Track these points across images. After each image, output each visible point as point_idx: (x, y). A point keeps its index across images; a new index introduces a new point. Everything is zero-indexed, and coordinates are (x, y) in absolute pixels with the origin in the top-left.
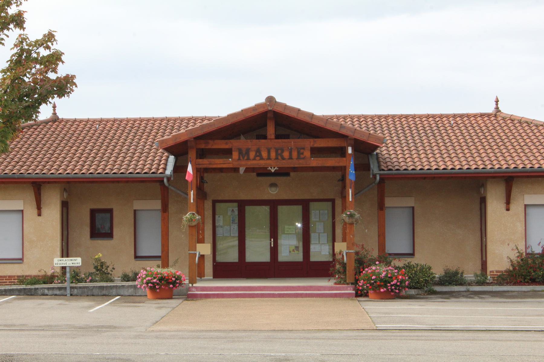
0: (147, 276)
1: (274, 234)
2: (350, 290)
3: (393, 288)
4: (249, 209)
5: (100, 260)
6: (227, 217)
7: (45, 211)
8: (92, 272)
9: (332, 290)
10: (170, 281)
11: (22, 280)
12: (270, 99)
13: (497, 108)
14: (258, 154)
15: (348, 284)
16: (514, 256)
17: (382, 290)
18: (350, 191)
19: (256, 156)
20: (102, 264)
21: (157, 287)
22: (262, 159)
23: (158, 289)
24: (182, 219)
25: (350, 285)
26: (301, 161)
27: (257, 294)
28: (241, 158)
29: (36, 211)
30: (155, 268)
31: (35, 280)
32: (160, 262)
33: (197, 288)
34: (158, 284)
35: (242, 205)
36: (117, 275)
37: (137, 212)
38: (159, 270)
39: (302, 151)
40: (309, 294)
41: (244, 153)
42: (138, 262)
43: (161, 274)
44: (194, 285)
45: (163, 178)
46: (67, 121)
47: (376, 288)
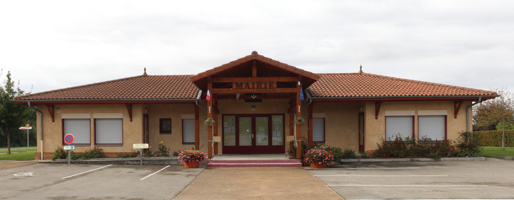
0: (184, 154)
1: (254, 131)
4: (241, 119)
6: (230, 122)
7: (134, 119)
11: (120, 155)
12: (255, 53)
13: (361, 71)
16: (380, 143)
20: (163, 147)
22: (249, 88)
26: (271, 90)
29: (129, 119)
30: (191, 150)
31: (127, 155)
32: (194, 146)
33: (213, 161)
34: (190, 159)
35: (238, 117)
38: (191, 151)
43: (192, 153)
46: (151, 76)
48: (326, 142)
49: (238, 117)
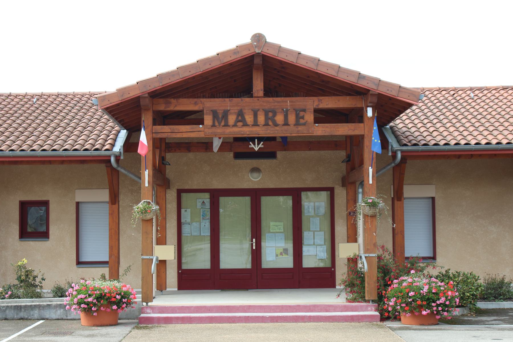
2: (371, 310)
3: (440, 308)
5: (25, 268)
8: (15, 284)
9: (346, 311)
10: (113, 299)
12: (258, 38)
14: (240, 118)
15: (368, 301)
17: (424, 313)
18: (371, 170)
19: (237, 121)
20: (28, 273)
21: (93, 309)
22: (245, 125)
23: (95, 311)
24: (133, 209)
25: (371, 304)
26: (300, 128)
27: (240, 317)
28: (217, 124)
30: (97, 281)
33: (154, 309)
34: (95, 305)
35: (216, 196)
36: (47, 289)
37: (80, 205)
39: (302, 114)
40: (314, 317)
41: (220, 116)
42: (81, 269)
43: (100, 289)
44: (150, 304)
45: (110, 156)
47: (415, 309)
48: (439, 259)
49: (216, 196)
